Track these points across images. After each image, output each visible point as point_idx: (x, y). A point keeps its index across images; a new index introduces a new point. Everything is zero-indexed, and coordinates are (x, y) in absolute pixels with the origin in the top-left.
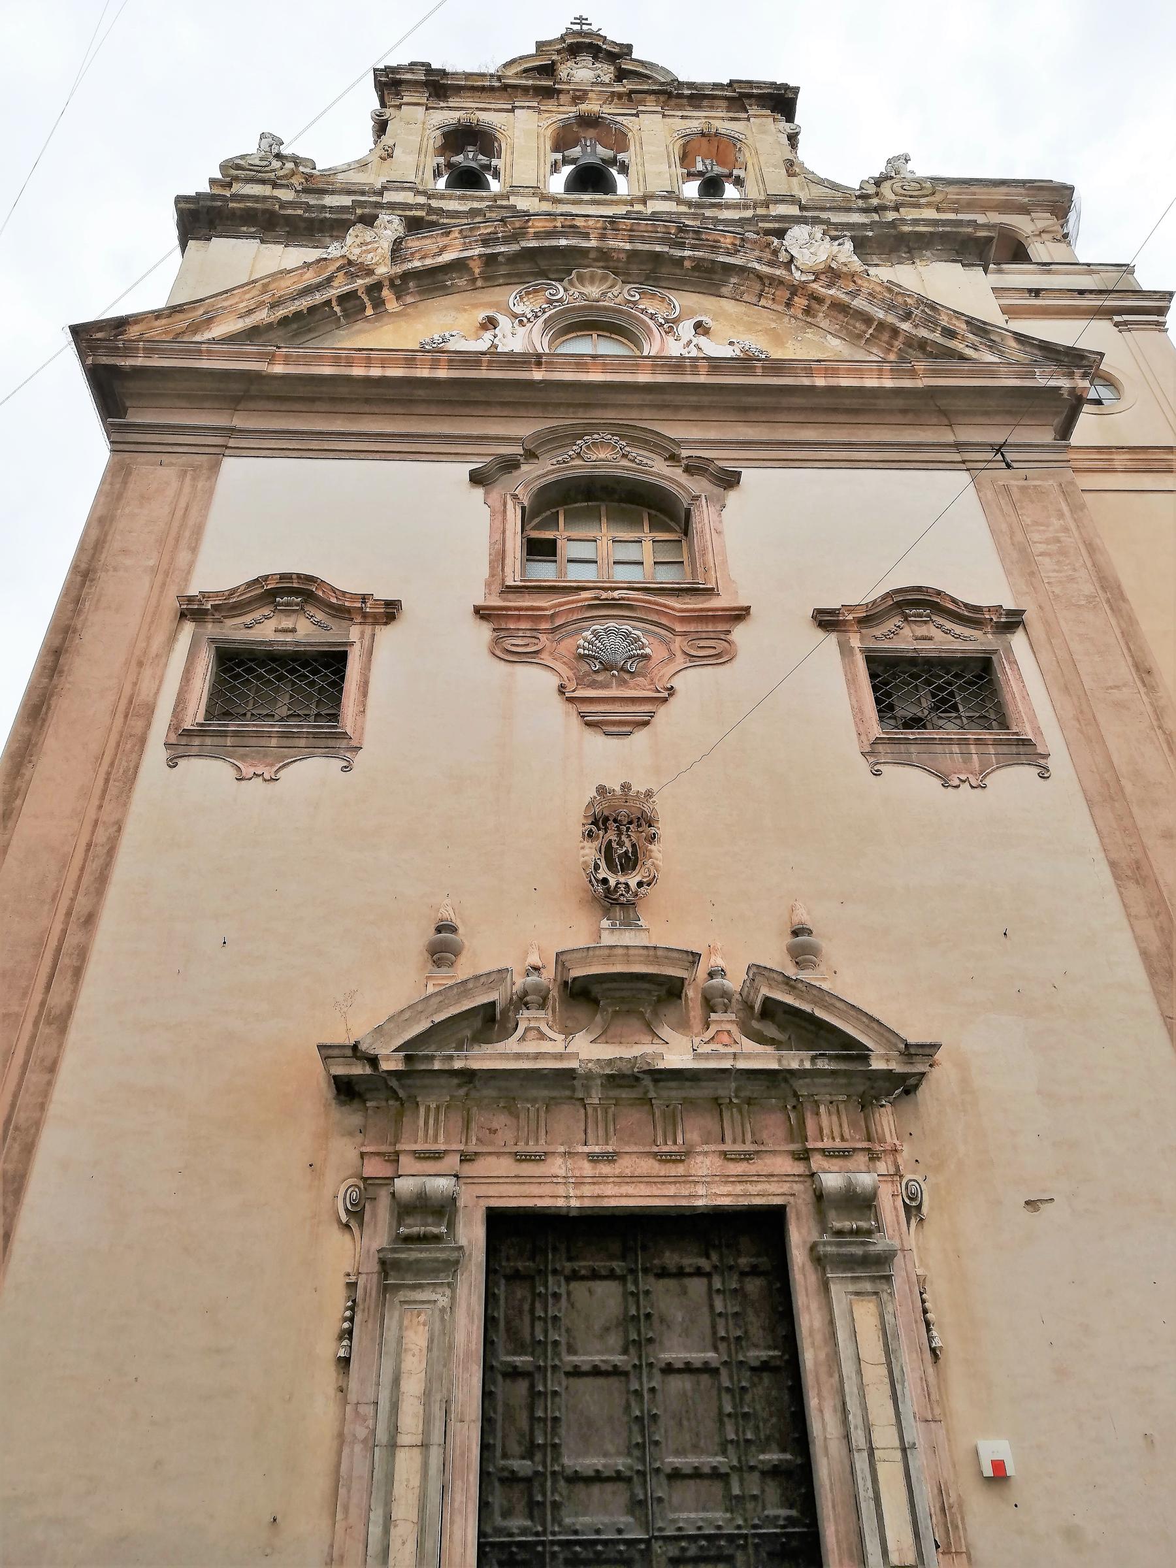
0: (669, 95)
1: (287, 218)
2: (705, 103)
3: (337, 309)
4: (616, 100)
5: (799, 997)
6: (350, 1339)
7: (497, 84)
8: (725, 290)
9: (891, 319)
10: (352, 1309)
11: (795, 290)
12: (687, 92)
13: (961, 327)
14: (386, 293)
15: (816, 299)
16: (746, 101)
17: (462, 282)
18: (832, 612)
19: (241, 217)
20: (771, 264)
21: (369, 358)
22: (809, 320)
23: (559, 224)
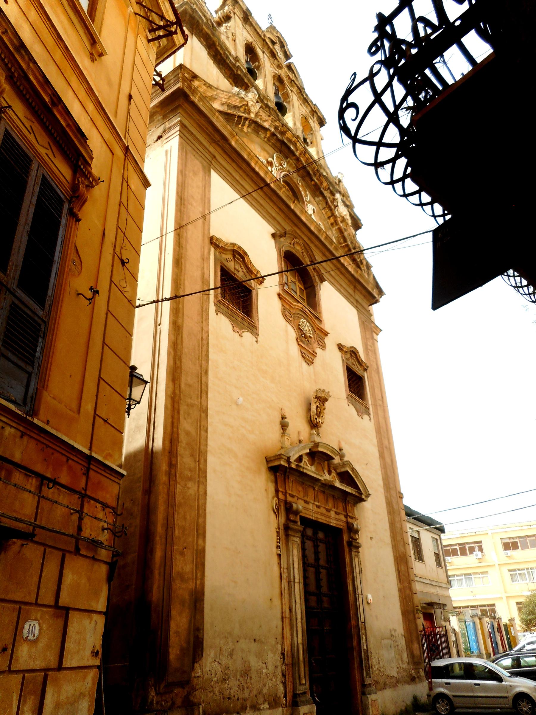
0: (301, 92)
1: (217, 49)
2: (306, 104)
3: (236, 119)
4: (287, 78)
5: (353, 473)
6: (280, 549)
7: (263, 37)
8: (316, 199)
9: (351, 246)
10: (279, 539)
11: (333, 215)
12: (305, 96)
13: (365, 263)
14: (247, 123)
15: (336, 222)
16: (315, 114)
17: (262, 136)
18: (343, 346)
19: (203, 34)
20: (331, 202)
21: (257, 162)
22: (331, 227)
23: (293, 140)
